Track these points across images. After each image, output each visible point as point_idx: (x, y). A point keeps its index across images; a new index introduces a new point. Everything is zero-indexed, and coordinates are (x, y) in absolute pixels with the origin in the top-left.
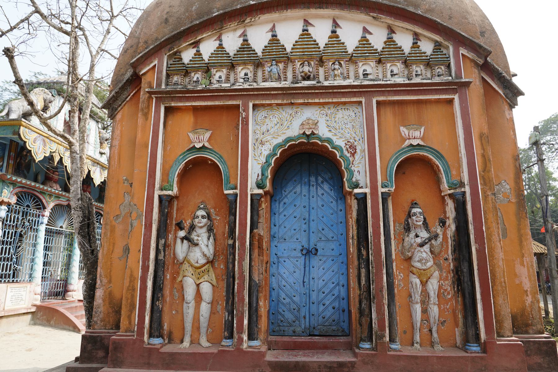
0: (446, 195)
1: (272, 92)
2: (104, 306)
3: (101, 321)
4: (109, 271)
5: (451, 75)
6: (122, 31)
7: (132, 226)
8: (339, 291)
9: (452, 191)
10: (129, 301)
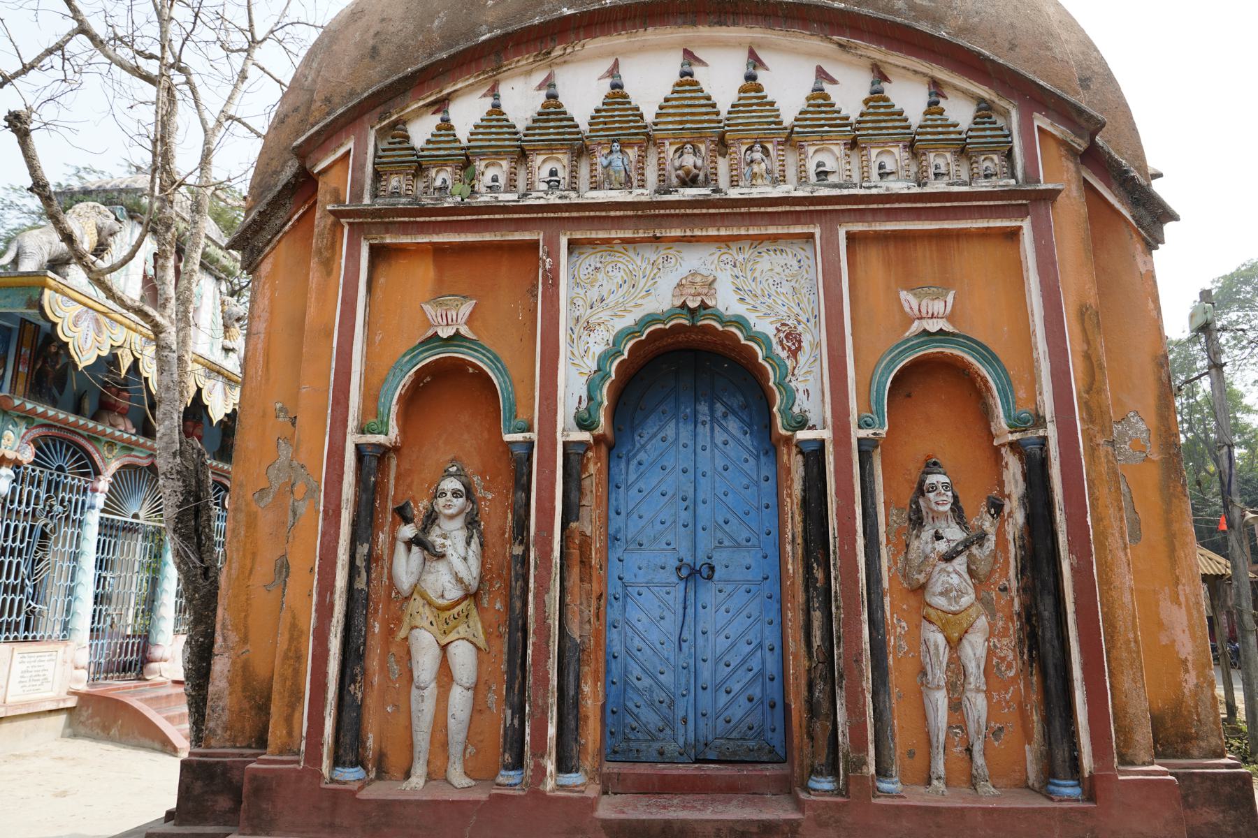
1: (612, 213)
2: (230, 694)
3: (225, 729)
5: (1013, 176)
8: (763, 662)
10: (288, 683)
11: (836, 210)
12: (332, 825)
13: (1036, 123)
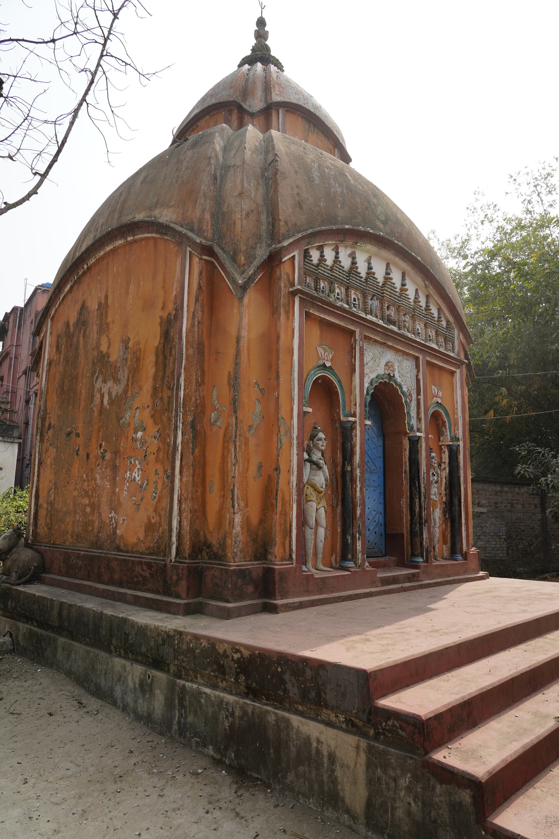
0: (444, 445)
1: (378, 329)
2: (242, 534)
3: (241, 552)
4: (245, 492)
5: (453, 352)
6: (86, 88)
7: (281, 443)
8: (379, 518)
9: (451, 443)
10: (283, 527)
11: (329, 310)
12: (307, 591)
13: (296, 253)
